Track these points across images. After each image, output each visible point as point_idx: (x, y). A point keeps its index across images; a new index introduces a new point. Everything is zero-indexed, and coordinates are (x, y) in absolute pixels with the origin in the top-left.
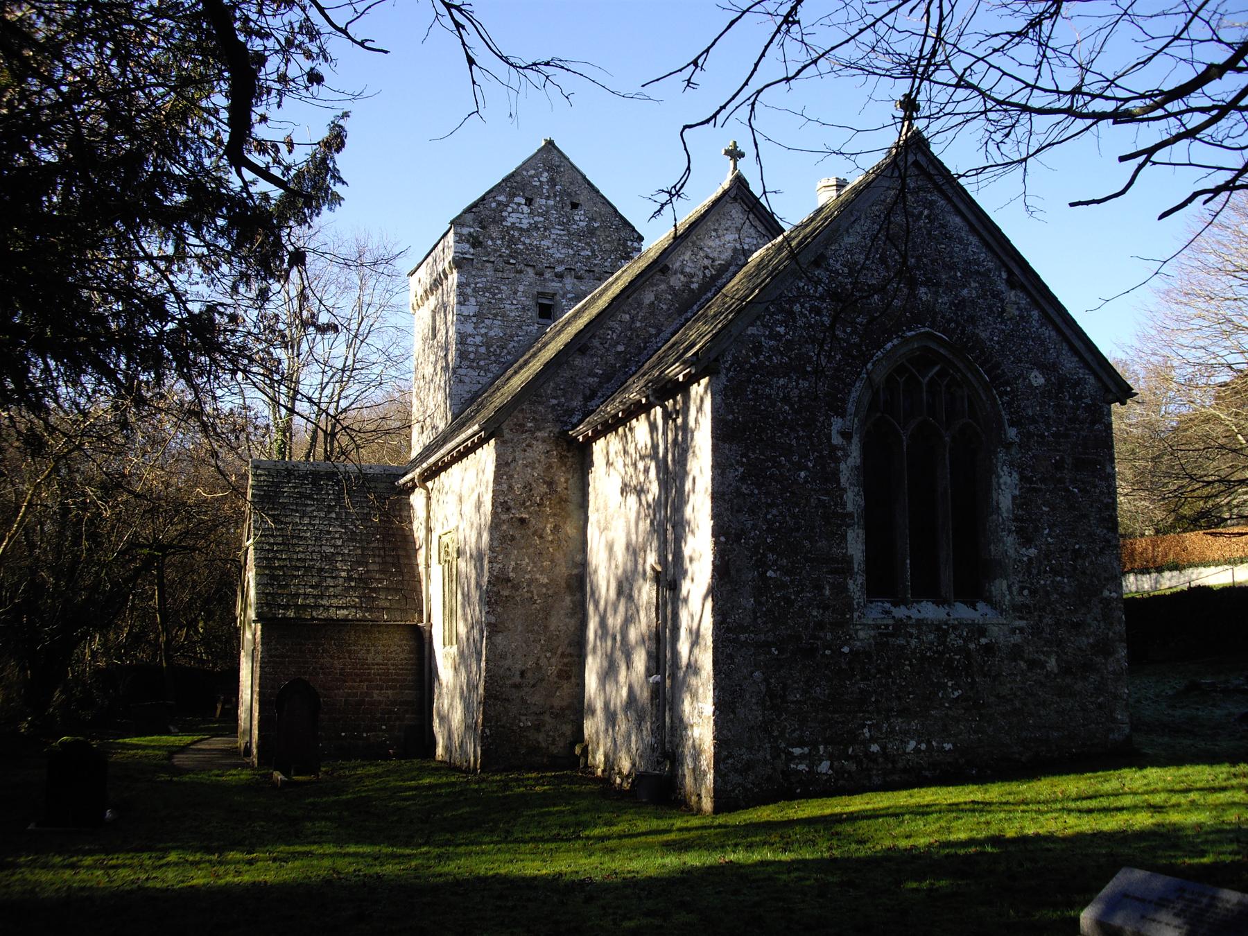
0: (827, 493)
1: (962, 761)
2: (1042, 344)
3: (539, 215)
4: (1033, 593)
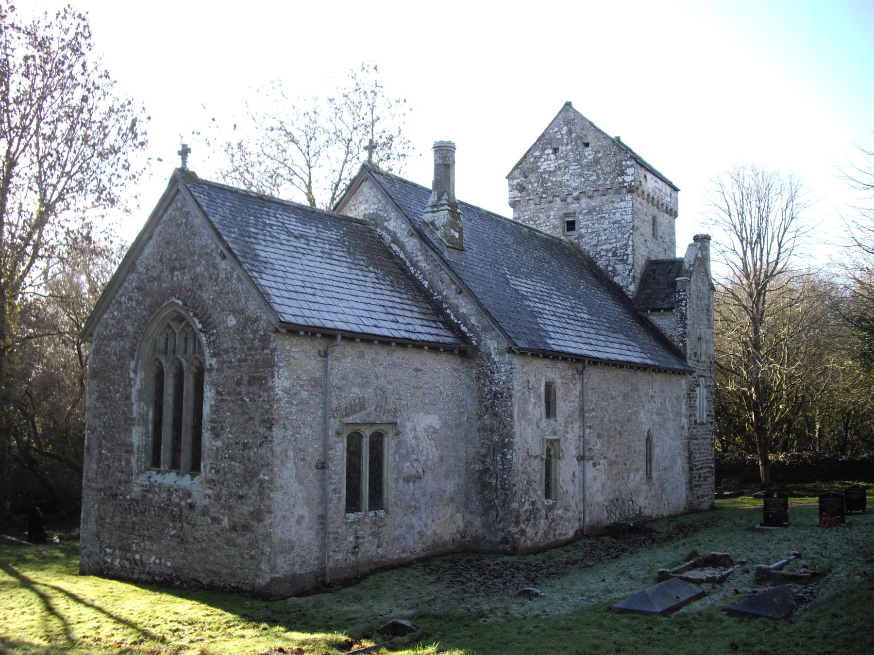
0: (126, 407)
1: (174, 575)
2: (237, 296)
3: (562, 158)
4: (217, 472)
